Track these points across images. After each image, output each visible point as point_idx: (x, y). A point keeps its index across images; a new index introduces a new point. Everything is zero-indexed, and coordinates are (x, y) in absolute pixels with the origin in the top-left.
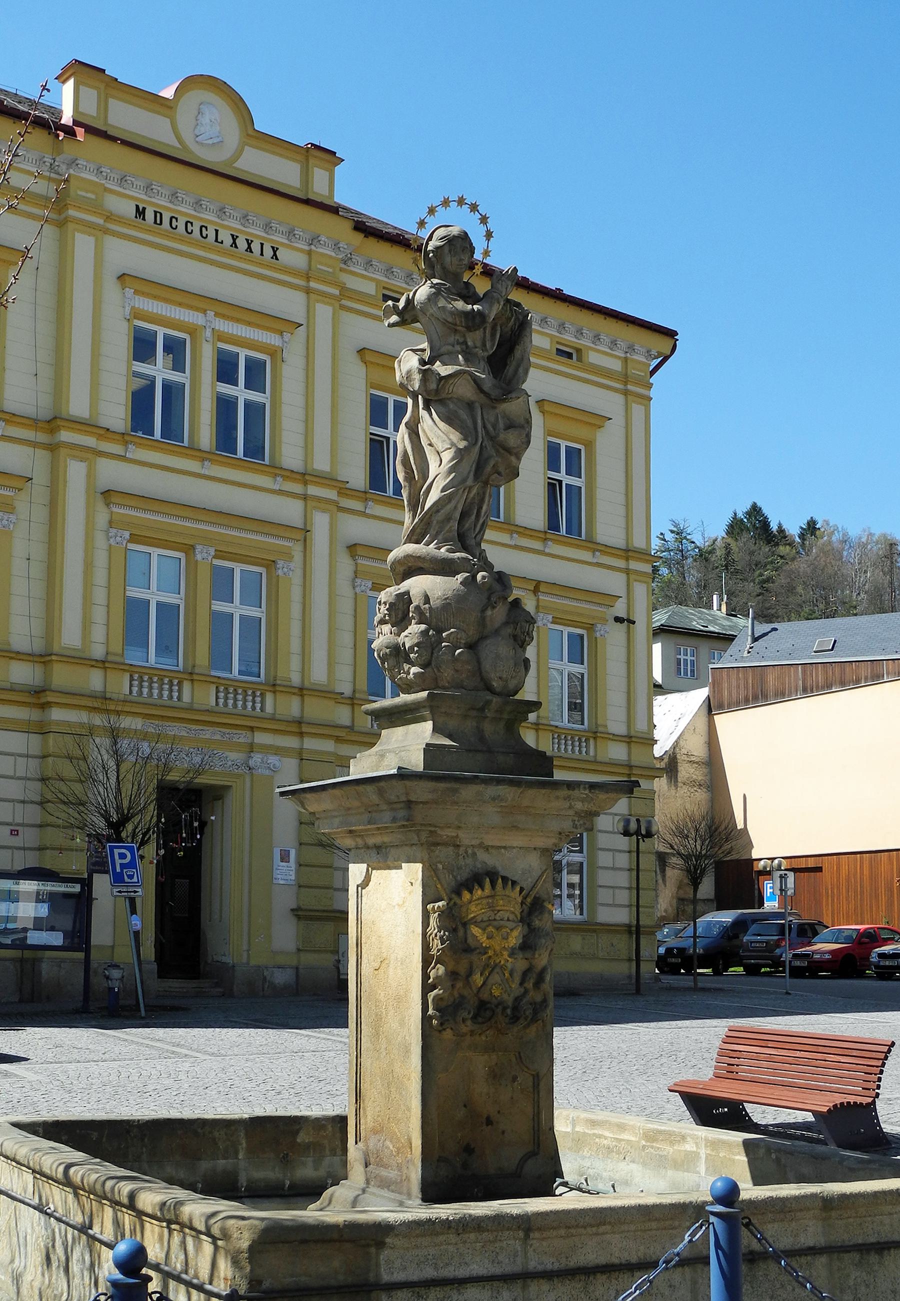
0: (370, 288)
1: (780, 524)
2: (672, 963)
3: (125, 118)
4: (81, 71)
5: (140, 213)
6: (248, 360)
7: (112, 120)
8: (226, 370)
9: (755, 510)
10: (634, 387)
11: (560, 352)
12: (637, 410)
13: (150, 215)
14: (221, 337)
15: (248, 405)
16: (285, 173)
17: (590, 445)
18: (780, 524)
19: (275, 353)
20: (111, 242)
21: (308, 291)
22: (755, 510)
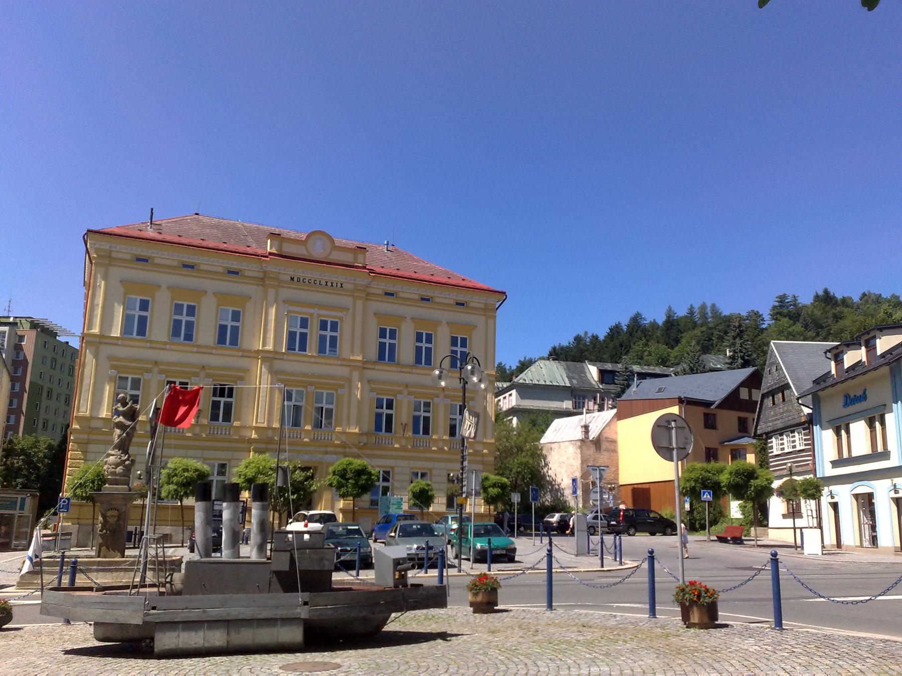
0: (380, 292)
1: (670, 309)
2: (347, 590)
3: (289, 249)
4: (274, 236)
5: (292, 279)
6: (332, 322)
7: (284, 249)
8: (323, 325)
9: (826, 292)
10: (490, 312)
11: (457, 304)
12: (491, 321)
13: (295, 279)
14: (319, 315)
15: (301, 334)
16: (348, 258)
17: (470, 336)
18: (670, 309)
19: (341, 319)
20: (281, 290)
21: (353, 296)
22: (826, 292)
